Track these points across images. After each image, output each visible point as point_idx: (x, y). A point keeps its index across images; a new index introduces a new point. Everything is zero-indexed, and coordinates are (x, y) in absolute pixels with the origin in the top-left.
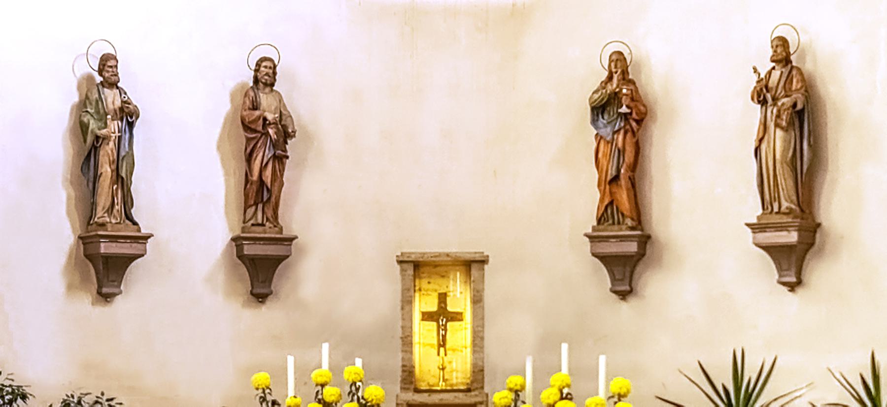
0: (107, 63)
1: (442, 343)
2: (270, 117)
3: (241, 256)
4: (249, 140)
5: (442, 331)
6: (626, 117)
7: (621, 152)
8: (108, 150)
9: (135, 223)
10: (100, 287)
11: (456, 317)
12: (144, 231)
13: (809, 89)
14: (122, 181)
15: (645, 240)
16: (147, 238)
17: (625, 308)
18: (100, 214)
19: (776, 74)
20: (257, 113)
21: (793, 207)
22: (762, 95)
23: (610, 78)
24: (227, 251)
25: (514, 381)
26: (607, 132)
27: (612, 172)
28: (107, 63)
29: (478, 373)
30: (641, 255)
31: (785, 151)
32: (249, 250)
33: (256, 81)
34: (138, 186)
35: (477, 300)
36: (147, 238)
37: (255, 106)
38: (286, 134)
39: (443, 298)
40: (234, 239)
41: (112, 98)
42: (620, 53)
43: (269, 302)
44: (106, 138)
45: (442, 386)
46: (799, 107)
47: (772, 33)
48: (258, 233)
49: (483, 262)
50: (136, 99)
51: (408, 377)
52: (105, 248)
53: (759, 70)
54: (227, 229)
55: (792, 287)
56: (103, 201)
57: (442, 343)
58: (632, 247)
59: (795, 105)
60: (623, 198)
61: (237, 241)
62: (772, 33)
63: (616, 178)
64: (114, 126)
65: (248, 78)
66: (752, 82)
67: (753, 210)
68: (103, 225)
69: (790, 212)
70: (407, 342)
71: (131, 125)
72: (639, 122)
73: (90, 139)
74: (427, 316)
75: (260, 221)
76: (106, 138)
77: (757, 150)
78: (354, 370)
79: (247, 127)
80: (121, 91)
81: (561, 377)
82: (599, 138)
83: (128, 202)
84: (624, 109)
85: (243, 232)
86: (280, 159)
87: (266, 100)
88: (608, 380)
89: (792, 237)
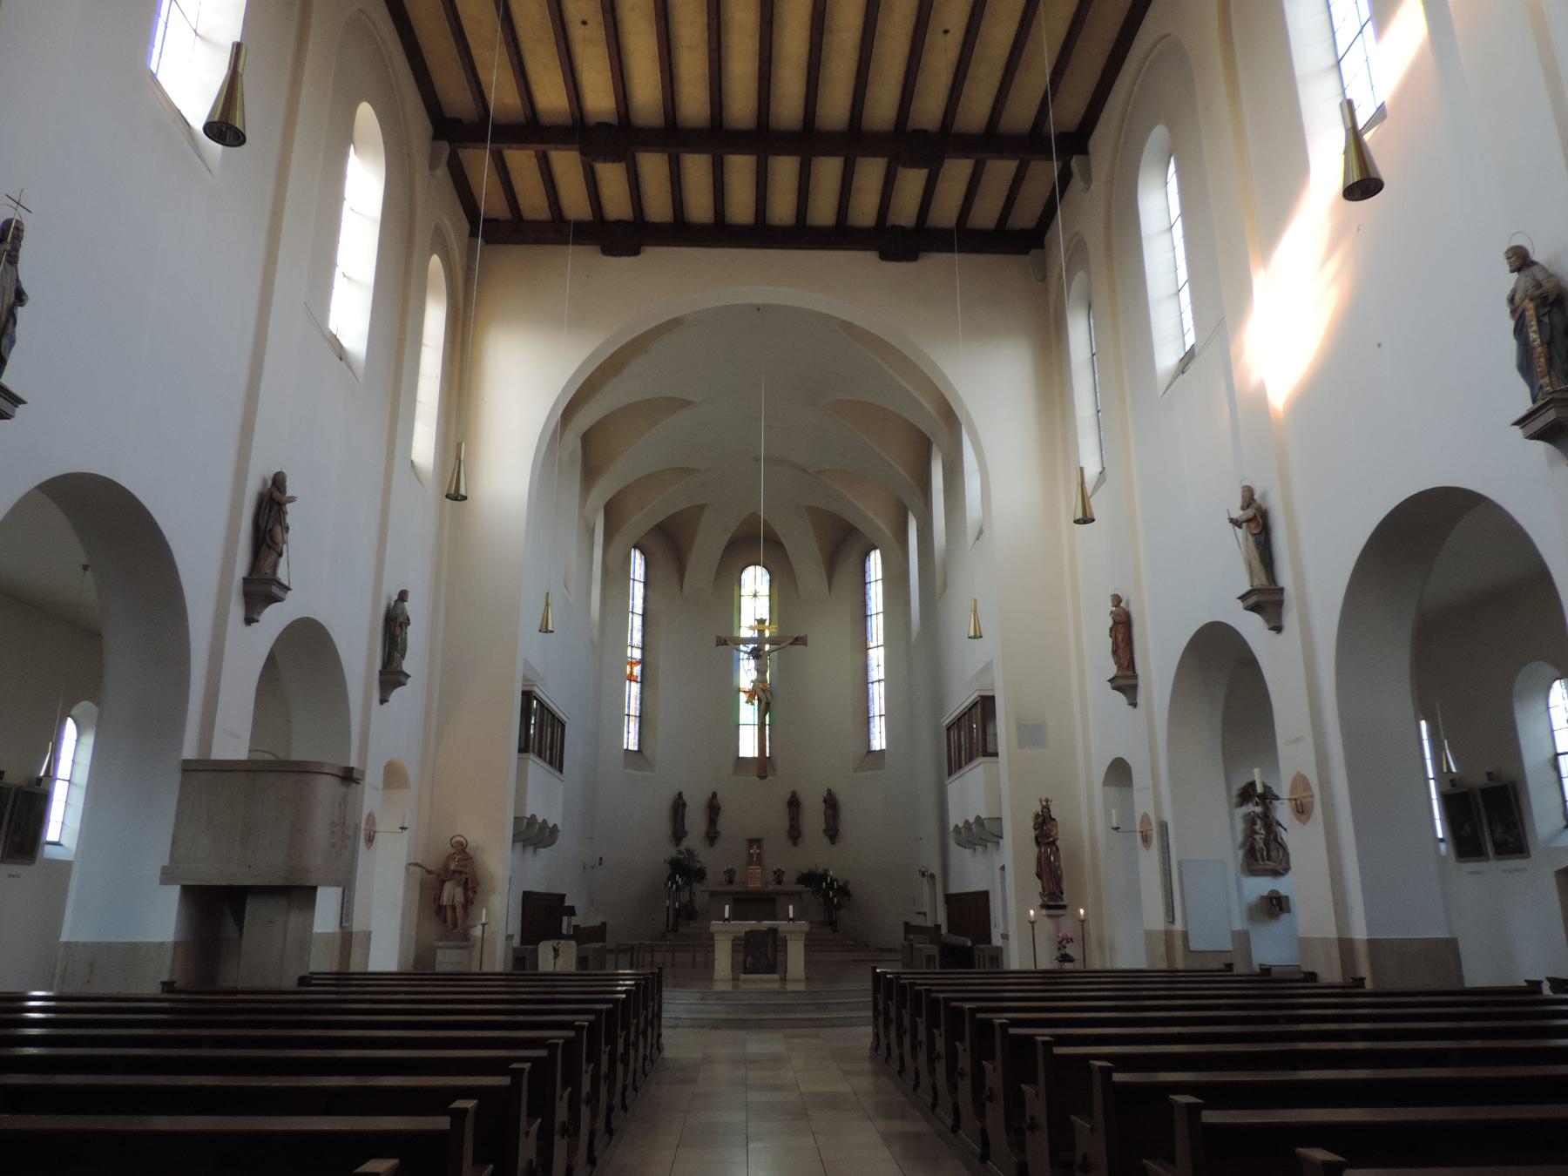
15: (800, 833)
22: (825, 801)
28: (680, 794)
30: (799, 836)
38: (719, 809)
41: (681, 802)
61: (707, 833)
65: (710, 796)
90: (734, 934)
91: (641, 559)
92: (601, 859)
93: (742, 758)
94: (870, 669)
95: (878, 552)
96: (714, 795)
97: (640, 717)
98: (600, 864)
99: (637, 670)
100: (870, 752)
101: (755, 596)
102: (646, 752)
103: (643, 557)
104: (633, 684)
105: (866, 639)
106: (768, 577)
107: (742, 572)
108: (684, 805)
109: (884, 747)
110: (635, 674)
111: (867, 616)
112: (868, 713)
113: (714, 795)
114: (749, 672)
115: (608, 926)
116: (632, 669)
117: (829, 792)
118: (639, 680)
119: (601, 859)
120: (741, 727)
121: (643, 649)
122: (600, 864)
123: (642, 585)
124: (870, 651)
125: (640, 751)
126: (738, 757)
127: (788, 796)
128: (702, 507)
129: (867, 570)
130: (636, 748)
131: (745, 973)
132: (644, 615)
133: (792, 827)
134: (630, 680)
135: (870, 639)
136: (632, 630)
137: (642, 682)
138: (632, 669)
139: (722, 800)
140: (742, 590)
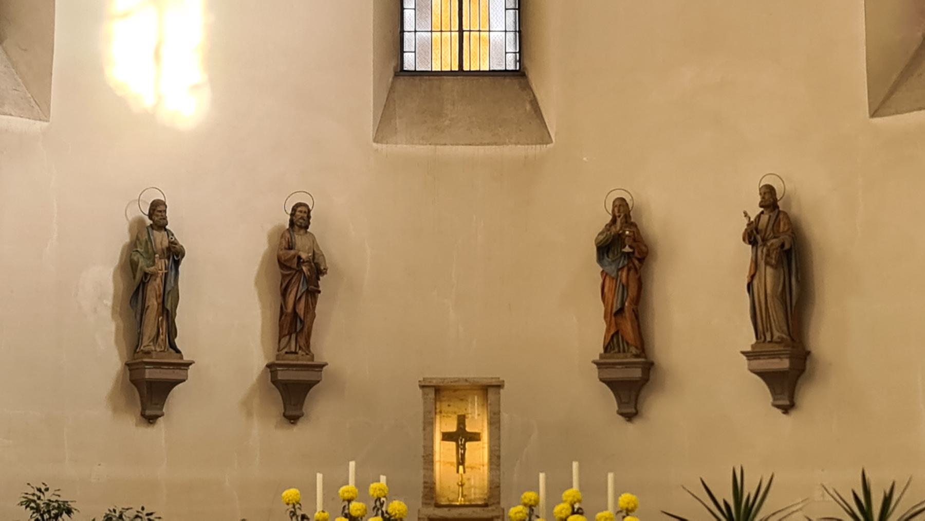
0: (157, 209)
1: (461, 461)
2: (304, 256)
3: (275, 381)
4: (284, 276)
5: (461, 448)
7: (625, 287)
8: (155, 286)
9: (178, 352)
10: (144, 409)
11: (475, 437)
12: (186, 358)
14: (168, 314)
15: (649, 367)
16: (188, 364)
17: (631, 429)
18: (146, 343)
19: (765, 218)
20: (292, 252)
21: (784, 336)
22: (752, 236)
23: (614, 221)
24: (261, 378)
25: (529, 496)
26: (611, 269)
27: (617, 306)
28: (157, 209)
29: (495, 488)
31: (775, 285)
32: (282, 375)
33: (292, 223)
34: (181, 320)
35: (495, 423)
36: (188, 364)
37: (290, 247)
38: (318, 271)
39: (461, 420)
40: (268, 366)
41: (160, 239)
43: (301, 423)
44: (154, 275)
45: (461, 501)
46: (787, 247)
48: (291, 360)
49: (499, 386)
50: (182, 240)
51: (430, 491)
52: (150, 374)
53: (749, 214)
55: (786, 410)
56: (149, 330)
57: (461, 461)
58: (637, 373)
59: (783, 245)
60: (628, 328)
63: (621, 311)
64: (161, 264)
66: (743, 225)
67: (748, 339)
68: (148, 353)
69: (781, 341)
70: (428, 459)
71: (177, 263)
72: (641, 260)
73: (139, 275)
74: (447, 437)
76: (154, 275)
77: (750, 286)
78: (379, 486)
79: (282, 264)
81: (573, 492)
82: (604, 274)
83: (172, 332)
84: (627, 249)
86: (313, 293)
87: (300, 240)
88: (617, 495)
89: (784, 364)
108: (175, 254)
133: (613, 343)
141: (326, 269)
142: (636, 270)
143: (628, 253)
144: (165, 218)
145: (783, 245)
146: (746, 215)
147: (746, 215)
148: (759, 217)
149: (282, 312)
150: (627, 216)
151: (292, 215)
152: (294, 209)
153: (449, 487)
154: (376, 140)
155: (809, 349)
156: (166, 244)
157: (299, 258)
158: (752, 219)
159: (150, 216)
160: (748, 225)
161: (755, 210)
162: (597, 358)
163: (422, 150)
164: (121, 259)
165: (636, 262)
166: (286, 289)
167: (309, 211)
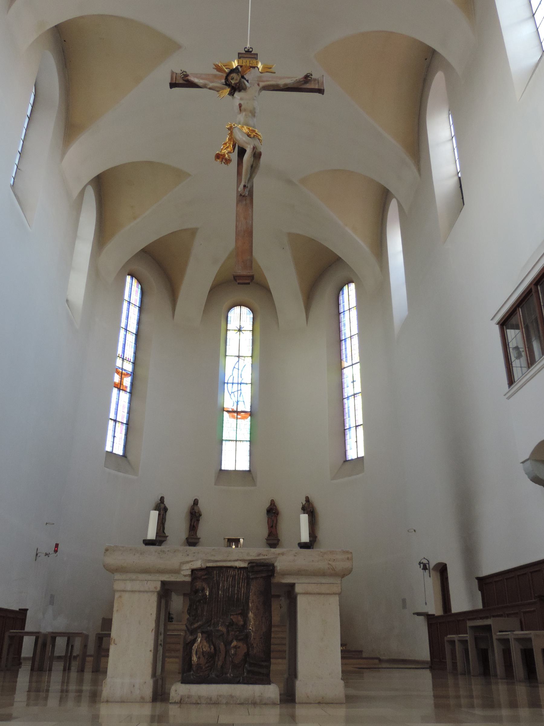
0: (162, 499)
2: (197, 511)
4: (191, 516)
6: (274, 513)
9: (165, 533)
13: (313, 507)
15: (279, 540)
16: (167, 536)
20: (194, 511)
21: (311, 532)
33: (194, 504)
36: (167, 536)
37: (193, 509)
38: (200, 515)
40: (186, 539)
41: (162, 506)
42: (273, 500)
46: (311, 511)
47: (229, 392)
53: (303, 503)
54: (200, 521)
59: (310, 510)
62: (229, 392)
63: (272, 527)
65: (192, 503)
66: (301, 506)
75: (193, 534)
80: (165, 505)
84: (274, 511)
85: (102, 631)
87: (195, 508)
90: (166, 578)
91: (137, 287)
92: (57, 545)
93: (224, 470)
94: (345, 386)
95: (352, 286)
96: (196, 502)
97: (127, 424)
98: (56, 551)
99: (127, 381)
100: (346, 461)
101: (240, 330)
102: (130, 457)
103: (140, 286)
104: (122, 393)
105: (341, 360)
106: (252, 316)
107: (229, 311)
109: (361, 454)
110: (124, 384)
111: (341, 341)
112: (344, 425)
113: (196, 502)
114: (232, 394)
115: (29, 613)
116: (121, 379)
117: (307, 500)
118: (128, 390)
119: (57, 545)
120: (224, 443)
121: (134, 363)
122: (56, 551)
123: (137, 309)
124: (345, 371)
125: (124, 456)
126: (221, 470)
127: (267, 505)
128: (193, 232)
129: (341, 302)
130: (121, 453)
131: (184, 681)
132: (137, 335)
133: (270, 534)
134: (119, 389)
135: (344, 360)
136: (124, 345)
137: (131, 393)
138: (121, 379)
139: (202, 506)
140: (228, 325)
141: (201, 515)
142: (276, 516)
143: (274, 513)
144: (164, 501)
145: (310, 510)
146: (302, 503)
147: (302, 503)
148: (305, 504)
149: (191, 525)
150: (274, 503)
151: (194, 501)
152: (195, 500)
153: (255, 708)
154: (215, 485)
155: (316, 535)
156: (163, 507)
157: (195, 512)
158: (304, 504)
159: (160, 500)
160: (303, 505)
161: (304, 502)
162: (266, 538)
163: (113, 472)
164: (503, 353)
165: (276, 515)
166: (192, 519)
167: (198, 501)
